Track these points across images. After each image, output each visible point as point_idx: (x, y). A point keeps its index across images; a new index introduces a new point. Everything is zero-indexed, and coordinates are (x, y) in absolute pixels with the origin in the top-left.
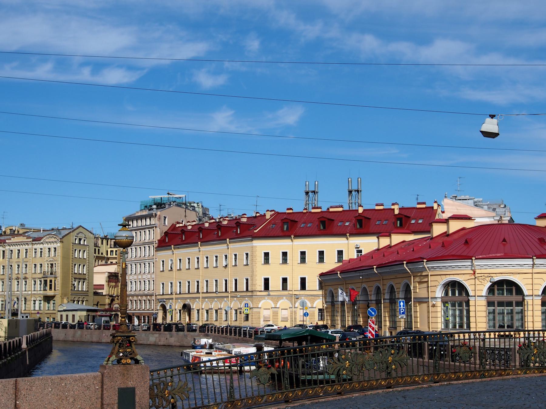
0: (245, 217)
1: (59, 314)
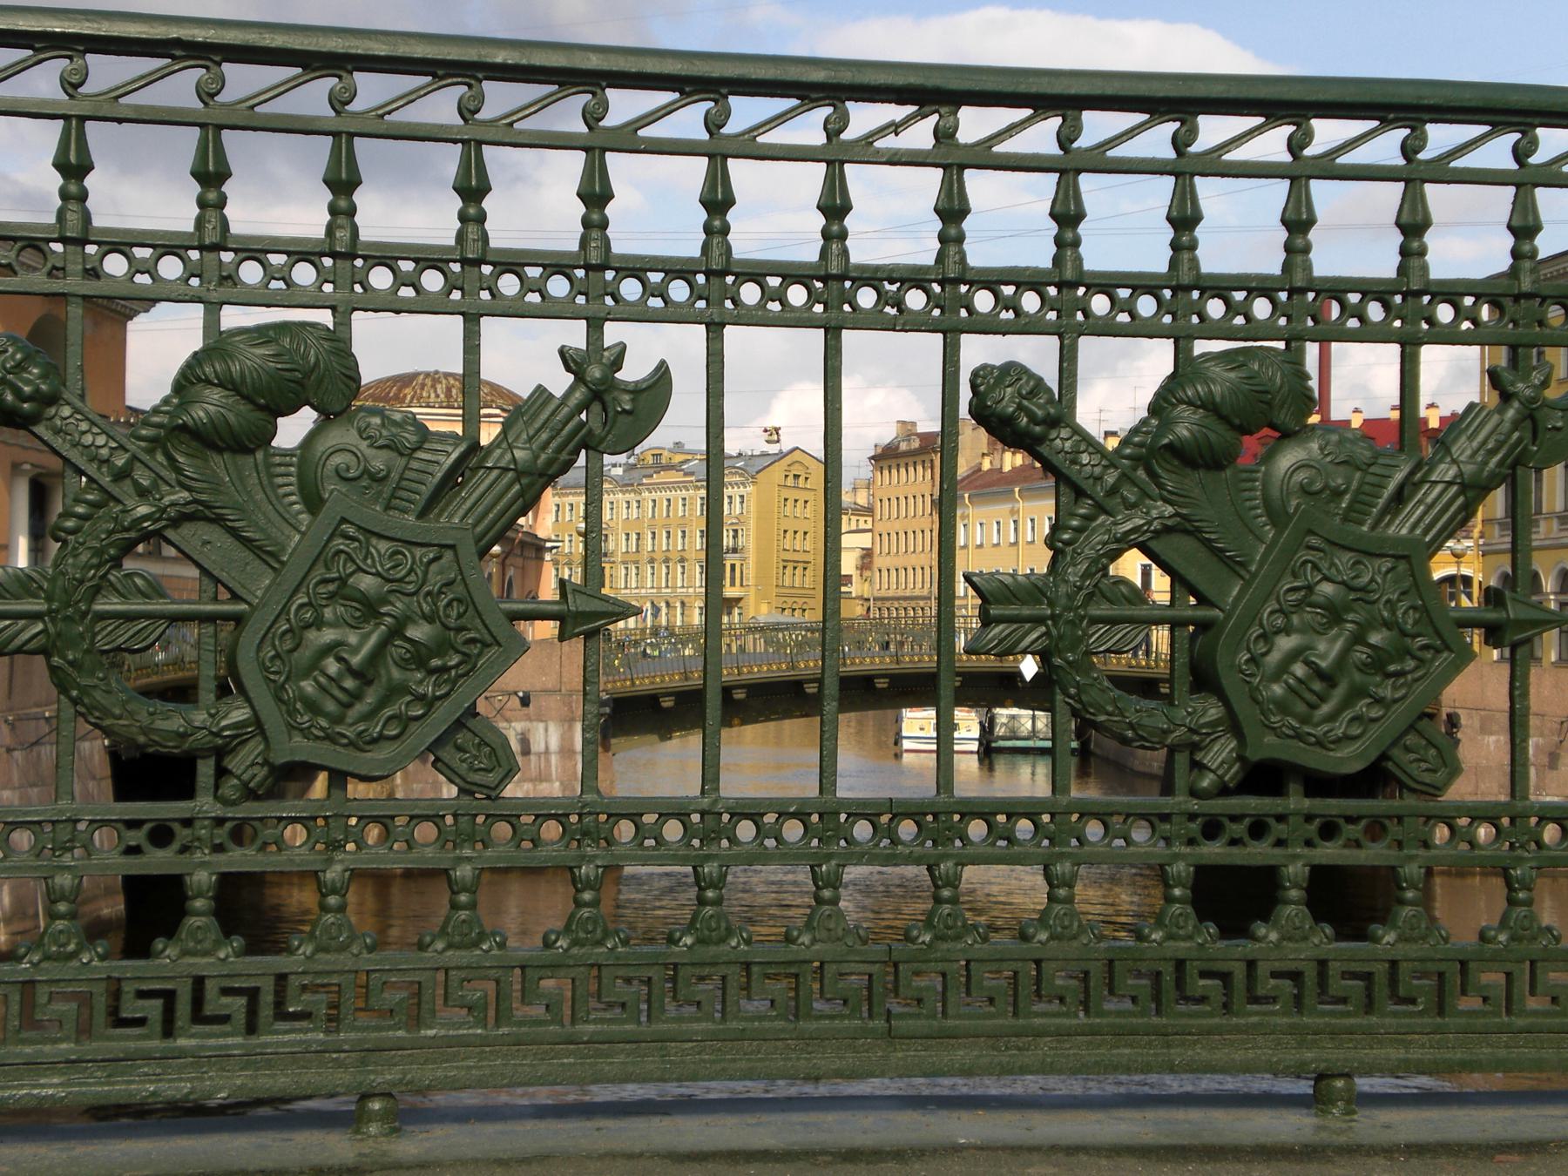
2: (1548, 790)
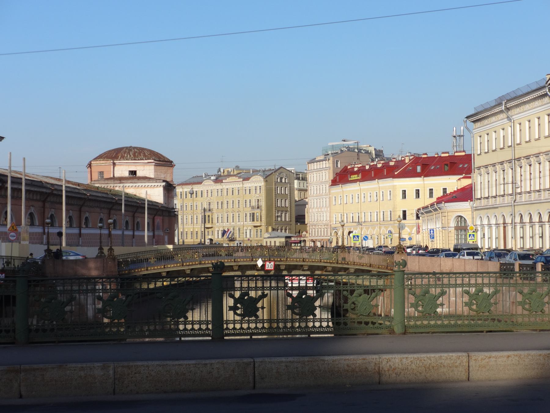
1: (265, 240)
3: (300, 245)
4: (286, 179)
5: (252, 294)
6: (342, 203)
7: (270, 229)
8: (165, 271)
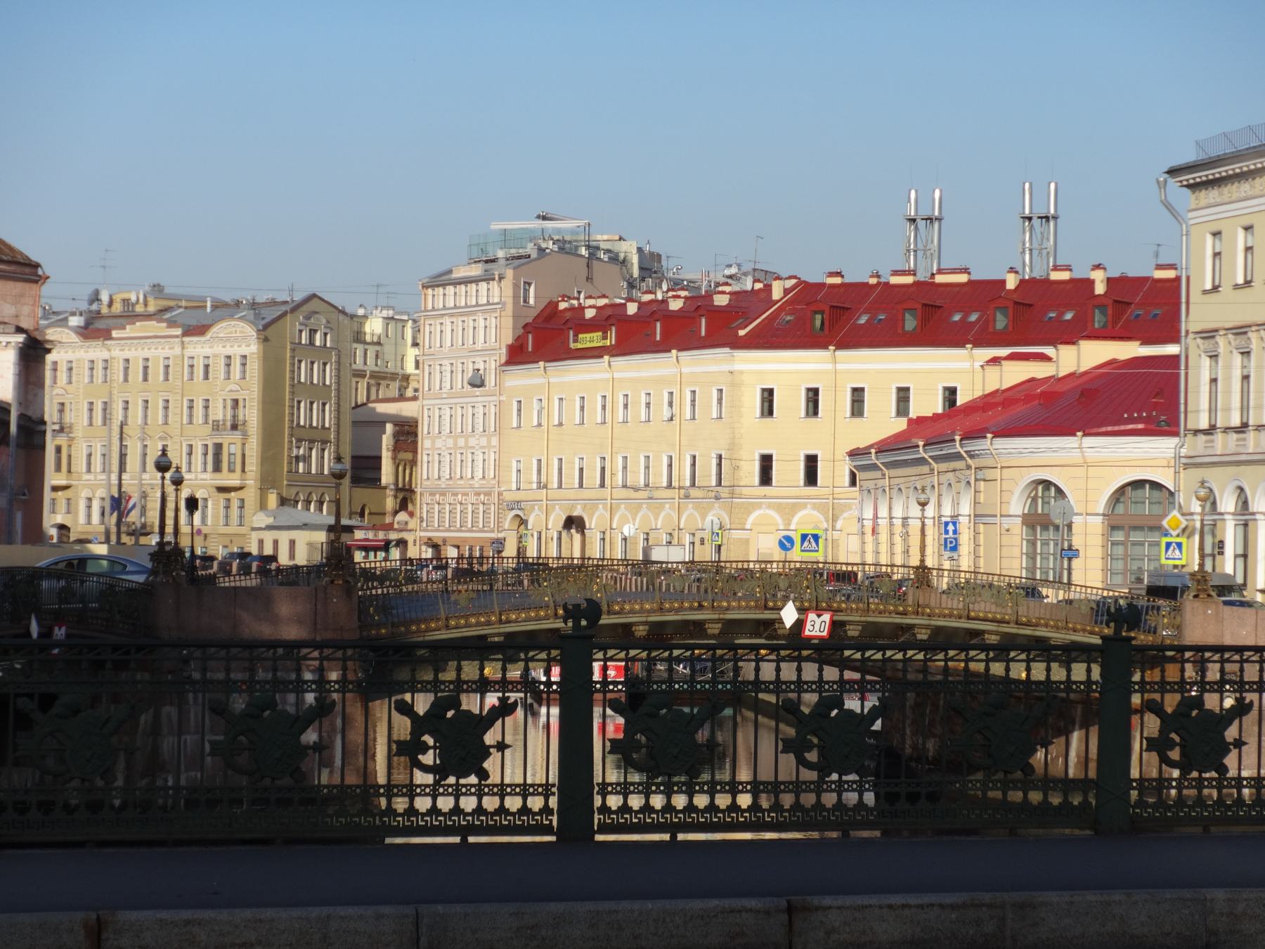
0: (723, 293)
1: (255, 536)
2: (1262, 775)
3: (383, 554)
4: (326, 334)
5: (471, 703)
6: (544, 422)
7: (272, 499)
8: (502, 630)
